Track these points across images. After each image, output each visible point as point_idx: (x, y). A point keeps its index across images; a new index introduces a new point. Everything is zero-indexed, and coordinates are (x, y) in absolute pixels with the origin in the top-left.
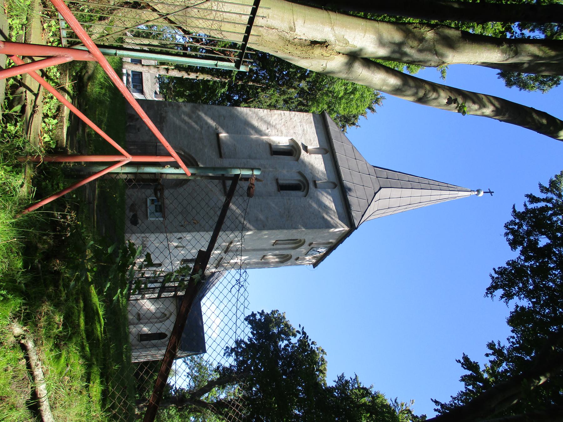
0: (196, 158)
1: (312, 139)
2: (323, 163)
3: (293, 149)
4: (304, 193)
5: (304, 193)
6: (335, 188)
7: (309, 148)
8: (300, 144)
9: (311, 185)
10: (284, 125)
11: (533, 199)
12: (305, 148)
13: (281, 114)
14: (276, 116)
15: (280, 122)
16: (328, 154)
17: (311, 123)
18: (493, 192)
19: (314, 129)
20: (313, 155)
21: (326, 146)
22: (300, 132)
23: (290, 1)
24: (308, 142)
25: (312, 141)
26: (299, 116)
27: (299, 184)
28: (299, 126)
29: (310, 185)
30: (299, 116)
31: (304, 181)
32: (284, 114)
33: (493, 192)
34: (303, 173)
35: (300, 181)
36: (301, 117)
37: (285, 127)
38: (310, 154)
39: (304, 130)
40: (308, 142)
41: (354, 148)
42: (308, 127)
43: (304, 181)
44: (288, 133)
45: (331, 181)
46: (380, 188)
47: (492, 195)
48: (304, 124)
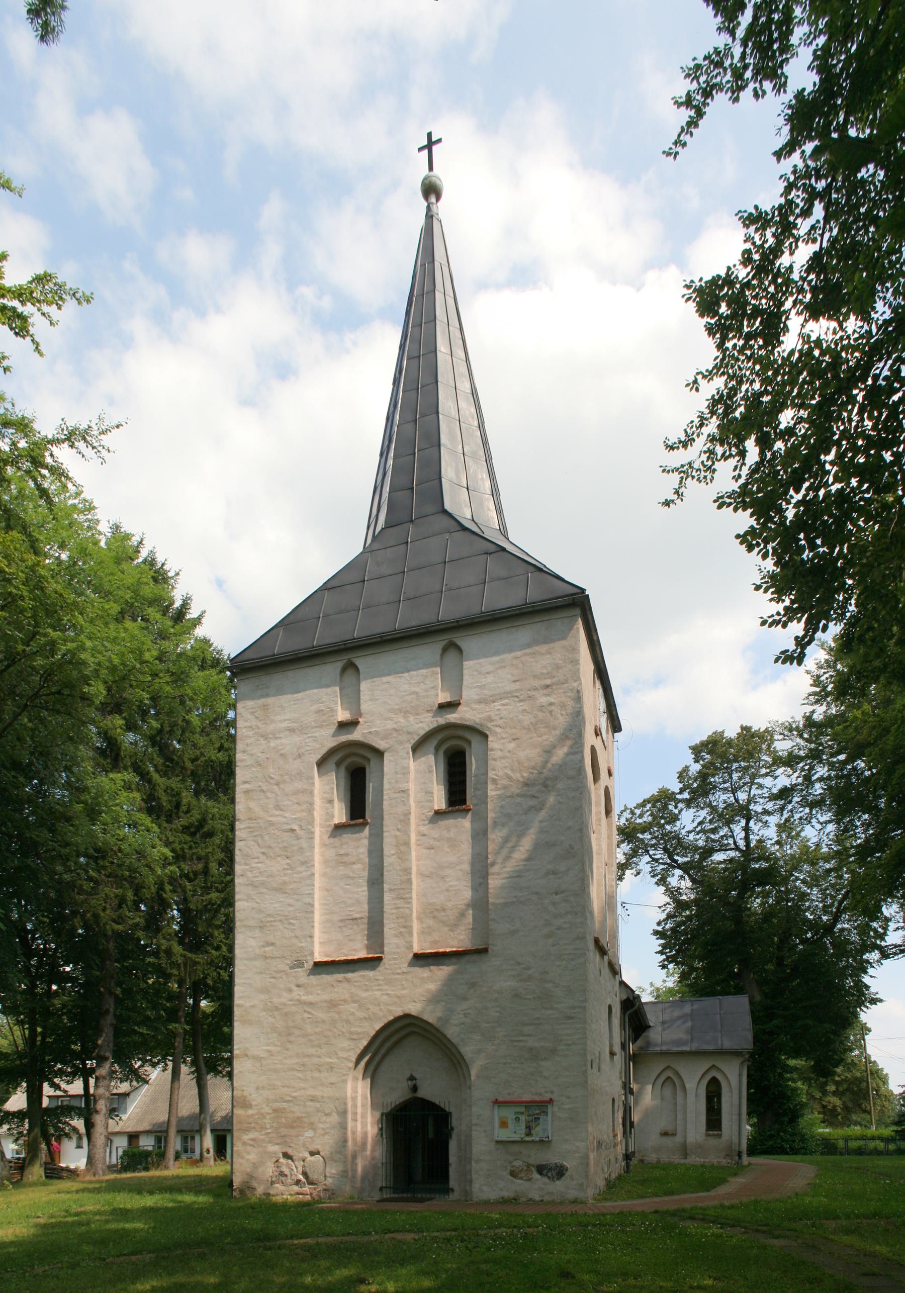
0: (386, 1021)
1: (315, 707)
2: (385, 679)
3: (346, 763)
4: (475, 741)
5: (475, 741)
6: (460, 650)
7: (343, 715)
8: (331, 743)
9: (452, 717)
10: (277, 784)
11: (37, 36)
12: (343, 726)
13: (247, 792)
14: (252, 805)
15: (269, 795)
16: (358, 662)
17: (265, 707)
18: (429, 135)
19: (285, 700)
20: (364, 707)
21: (333, 668)
22: (297, 739)
23: (365, 776)
24: (324, 718)
25: (322, 707)
26: (248, 741)
27: (445, 752)
28: (278, 742)
29: (453, 721)
30: (248, 741)
31: (439, 737)
32: (245, 782)
33: (429, 135)
34: (417, 738)
35: (437, 749)
36: (251, 733)
37: (284, 782)
38: (361, 715)
39: (292, 730)
40: (324, 718)
41: (329, 586)
42: (279, 718)
43: (439, 737)
44: (300, 774)
45: (438, 657)
46: (445, 512)
47: (439, 141)
48: (272, 727)
